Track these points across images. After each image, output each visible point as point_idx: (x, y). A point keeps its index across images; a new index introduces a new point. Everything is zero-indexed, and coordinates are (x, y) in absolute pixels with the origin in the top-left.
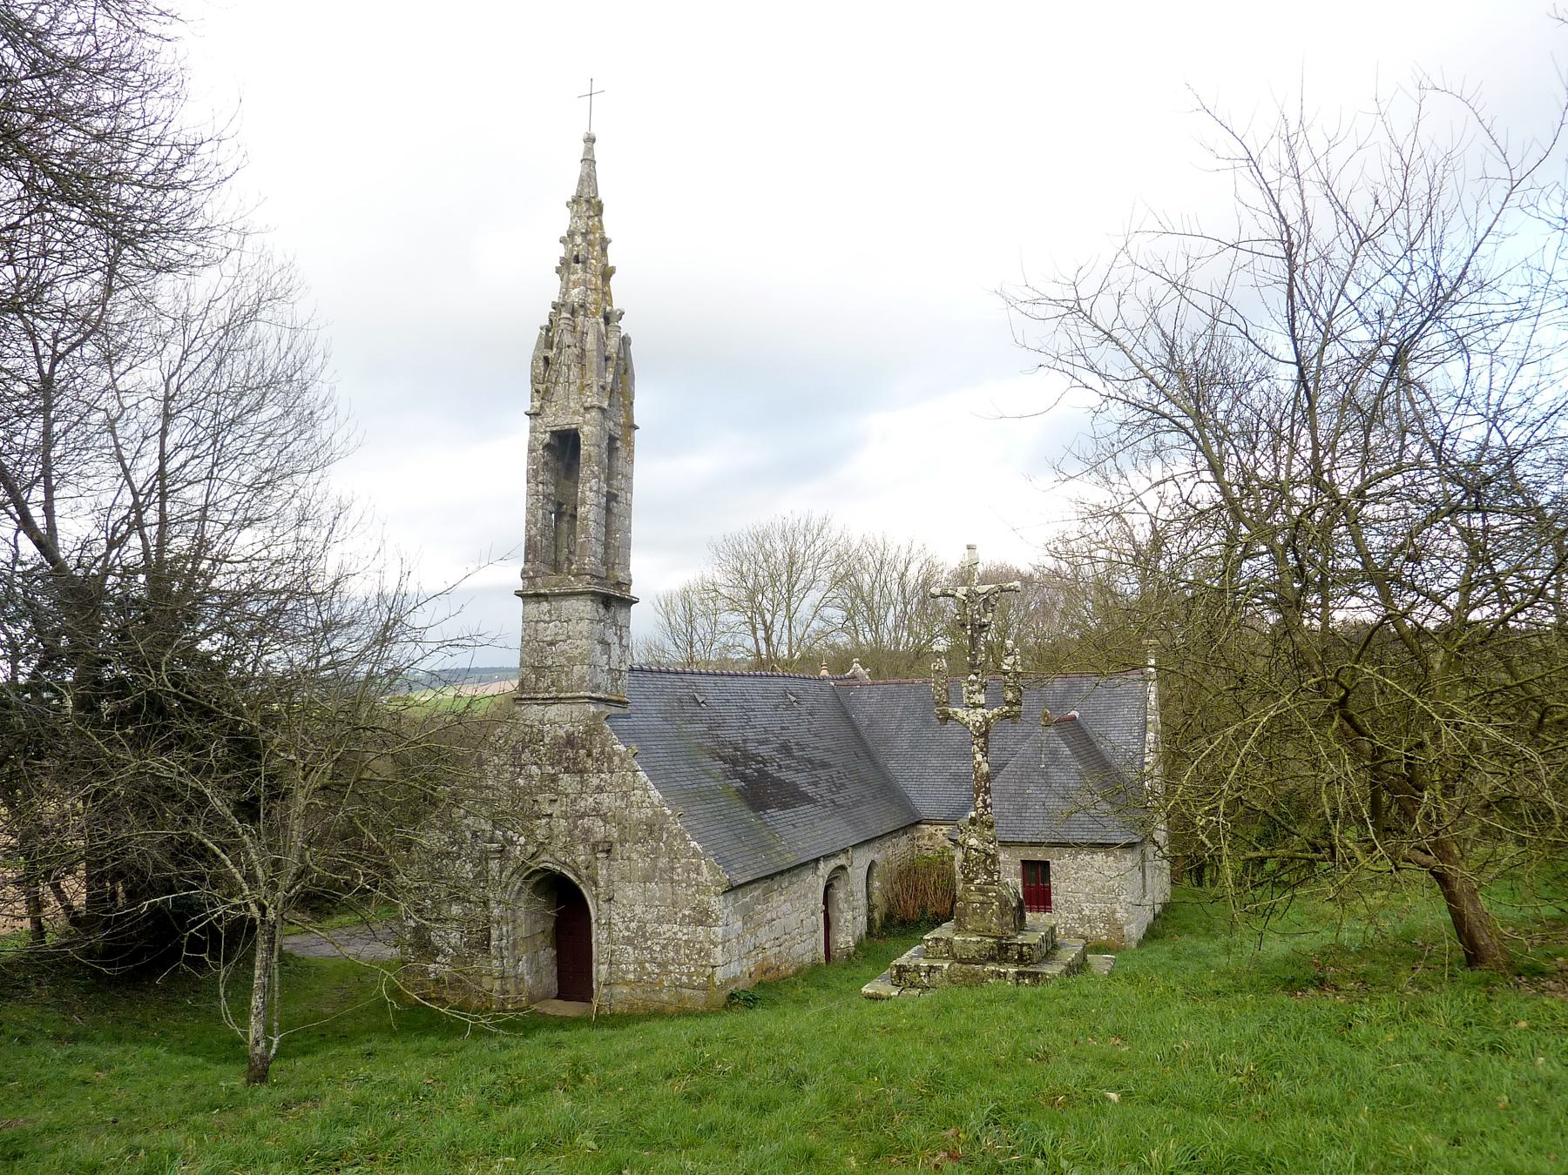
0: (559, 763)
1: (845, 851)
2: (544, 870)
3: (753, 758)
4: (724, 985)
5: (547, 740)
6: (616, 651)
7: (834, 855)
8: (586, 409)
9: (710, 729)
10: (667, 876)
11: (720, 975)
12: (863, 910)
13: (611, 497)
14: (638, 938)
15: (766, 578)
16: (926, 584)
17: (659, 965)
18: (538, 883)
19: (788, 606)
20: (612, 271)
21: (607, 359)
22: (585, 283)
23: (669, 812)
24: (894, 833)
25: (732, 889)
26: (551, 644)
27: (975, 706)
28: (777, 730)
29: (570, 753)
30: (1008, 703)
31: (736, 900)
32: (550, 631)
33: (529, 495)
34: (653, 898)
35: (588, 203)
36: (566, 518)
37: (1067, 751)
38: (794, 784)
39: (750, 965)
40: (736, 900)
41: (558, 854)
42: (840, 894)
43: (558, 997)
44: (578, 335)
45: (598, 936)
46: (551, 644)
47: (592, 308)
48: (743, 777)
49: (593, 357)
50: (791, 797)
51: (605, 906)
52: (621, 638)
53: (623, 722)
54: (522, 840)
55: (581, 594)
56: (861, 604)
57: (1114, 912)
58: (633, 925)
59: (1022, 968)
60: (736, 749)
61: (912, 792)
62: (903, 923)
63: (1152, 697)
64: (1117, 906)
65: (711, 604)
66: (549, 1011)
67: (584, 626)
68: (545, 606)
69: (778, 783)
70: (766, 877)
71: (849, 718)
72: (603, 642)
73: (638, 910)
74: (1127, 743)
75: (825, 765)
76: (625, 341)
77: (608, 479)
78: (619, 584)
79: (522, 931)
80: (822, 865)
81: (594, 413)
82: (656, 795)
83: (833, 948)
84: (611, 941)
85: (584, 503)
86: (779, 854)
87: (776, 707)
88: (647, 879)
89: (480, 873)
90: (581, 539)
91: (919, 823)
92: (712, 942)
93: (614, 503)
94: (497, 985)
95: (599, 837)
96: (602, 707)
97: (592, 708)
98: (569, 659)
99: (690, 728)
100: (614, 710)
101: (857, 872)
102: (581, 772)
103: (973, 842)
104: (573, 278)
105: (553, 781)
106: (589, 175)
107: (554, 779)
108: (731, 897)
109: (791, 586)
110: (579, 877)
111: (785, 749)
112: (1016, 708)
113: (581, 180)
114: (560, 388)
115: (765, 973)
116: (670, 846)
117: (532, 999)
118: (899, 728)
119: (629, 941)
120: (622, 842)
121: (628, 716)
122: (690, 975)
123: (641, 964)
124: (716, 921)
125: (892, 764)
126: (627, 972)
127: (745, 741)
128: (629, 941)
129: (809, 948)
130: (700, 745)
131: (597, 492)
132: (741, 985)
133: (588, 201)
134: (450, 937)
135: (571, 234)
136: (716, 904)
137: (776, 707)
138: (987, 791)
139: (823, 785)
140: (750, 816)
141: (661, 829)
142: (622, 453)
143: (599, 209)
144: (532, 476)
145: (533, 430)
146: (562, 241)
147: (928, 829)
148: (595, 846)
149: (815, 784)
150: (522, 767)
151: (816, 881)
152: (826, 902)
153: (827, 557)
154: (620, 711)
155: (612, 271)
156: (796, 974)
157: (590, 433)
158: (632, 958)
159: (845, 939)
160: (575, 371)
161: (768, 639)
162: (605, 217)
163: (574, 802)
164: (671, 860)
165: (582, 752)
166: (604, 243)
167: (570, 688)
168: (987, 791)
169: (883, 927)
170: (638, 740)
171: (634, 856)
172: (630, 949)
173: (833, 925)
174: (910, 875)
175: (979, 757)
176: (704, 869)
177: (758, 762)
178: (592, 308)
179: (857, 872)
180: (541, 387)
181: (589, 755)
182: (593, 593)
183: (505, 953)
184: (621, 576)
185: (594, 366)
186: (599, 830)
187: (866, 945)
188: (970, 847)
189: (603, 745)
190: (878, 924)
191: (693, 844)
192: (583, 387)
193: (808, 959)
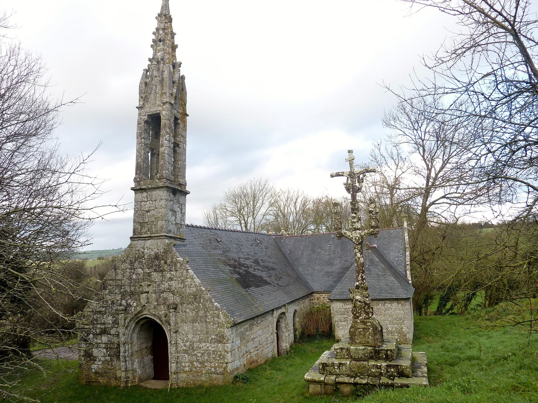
0: (152, 267)
1: (284, 306)
2: (146, 318)
3: (243, 265)
4: (232, 373)
5: (146, 257)
6: (179, 215)
7: (280, 308)
8: (164, 104)
9: (224, 252)
10: (204, 320)
11: (230, 367)
12: (292, 331)
13: (176, 145)
14: (190, 350)
15: (245, 202)
16: (304, 205)
17: (200, 363)
18: (143, 325)
19: (254, 214)
20: (176, 46)
21: (174, 82)
22: (164, 50)
23: (204, 289)
24: (303, 298)
25: (235, 325)
26: (148, 211)
27: (356, 229)
28: (253, 254)
29: (157, 262)
30: (372, 227)
31: (237, 330)
32: (147, 205)
33: (138, 144)
34: (197, 330)
35: (165, 17)
36: (156, 156)
37: (377, 260)
38: (261, 277)
39: (244, 361)
40: (237, 330)
41: (152, 311)
42: (283, 325)
43: (154, 378)
44: (160, 72)
45: (171, 349)
46: (148, 211)
47: (167, 61)
48: (239, 273)
49: (167, 81)
50: (260, 282)
51: (174, 335)
52: (181, 209)
53: (183, 248)
54: (135, 304)
55: (161, 187)
56: (281, 215)
57: (402, 328)
58: (188, 344)
59: (388, 363)
60: (235, 261)
61: (309, 279)
62: (309, 336)
63: (407, 238)
64: (403, 326)
65: (224, 215)
66: (149, 386)
67: (163, 203)
68: (145, 194)
69: (254, 276)
70: (251, 319)
71: (282, 251)
72: (172, 210)
73: (190, 336)
74: (398, 257)
75: (273, 269)
76: (183, 78)
77: (175, 137)
78: (180, 185)
79: (136, 348)
80: (275, 312)
81: (167, 105)
82: (197, 281)
83: (280, 349)
84: (177, 352)
85: (162, 146)
86: (256, 308)
87: (252, 245)
88: (194, 321)
89: (115, 321)
90: (161, 162)
91: (313, 293)
92: (226, 351)
93: (177, 148)
94: (123, 375)
95: (171, 302)
96: (172, 241)
97: (167, 241)
98: (156, 218)
99: (215, 252)
100: (178, 242)
101: (290, 315)
102: (162, 271)
103: (358, 297)
104: (158, 48)
105: (149, 276)
106: (165, 5)
107: (149, 275)
108: (234, 329)
109: (254, 207)
110: (161, 321)
111: (256, 262)
112: (377, 230)
113: (162, 7)
114: (152, 96)
115: (251, 364)
116: (204, 305)
117: (141, 380)
118: (302, 254)
119: (186, 352)
120: (182, 304)
121: (185, 246)
122: (215, 368)
123: (192, 363)
124: (227, 341)
125: (300, 269)
126: (185, 367)
127: (239, 258)
128: (186, 352)
129: (270, 351)
130: (219, 259)
131: (169, 141)
132: (240, 371)
133: (165, 15)
134: (99, 353)
135: (157, 29)
136: (227, 332)
137: (252, 245)
138: (363, 272)
139: (273, 277)
140: (243, 291)
141: (200, 297)
142: (181, 126)
143: (170, 20)
144: (139, 135)
145: (140, 115)
146: (154, 33)
147: (316, 296)
148: (169, 306)
149: (270, 277)
150: (134, 269)
151: (272, 319)
152: (277, 329)
153: (267, 195)
154: (182, 243)
155: (176, 46)
156: (265, 363)
157: (165, 114)
158: (187, 360)
159: (286, 345)
160: (159, 87)
161: (246, 227)
162: (174, 24)
163: (159, 285)
164: (205, 312)
165: (162, 262)
166: (173, 34)
167: (157, 232)
168: (363, 272)
169: (300, 338)
170: (189, 256)
171: (188, 310)
172: (186, 356)
173: (280, 338)
174: (310, 315)
175: (359, 255)
176: (221, 316)
177: (245, 267)
178: (167, 61)
179: (290, 315)
180: (143, 96)
181: (166, 263)
182: (167, 187)
183: (127, 359)
184: (181, 181)
185: (168, 85)
186: (171, 299)
187: (294, 346)
188: (357, 300)
189: (172, 258)
190: (298, 337)
191: (216, 304)
192: (162, 94)
193: (270, 355)
